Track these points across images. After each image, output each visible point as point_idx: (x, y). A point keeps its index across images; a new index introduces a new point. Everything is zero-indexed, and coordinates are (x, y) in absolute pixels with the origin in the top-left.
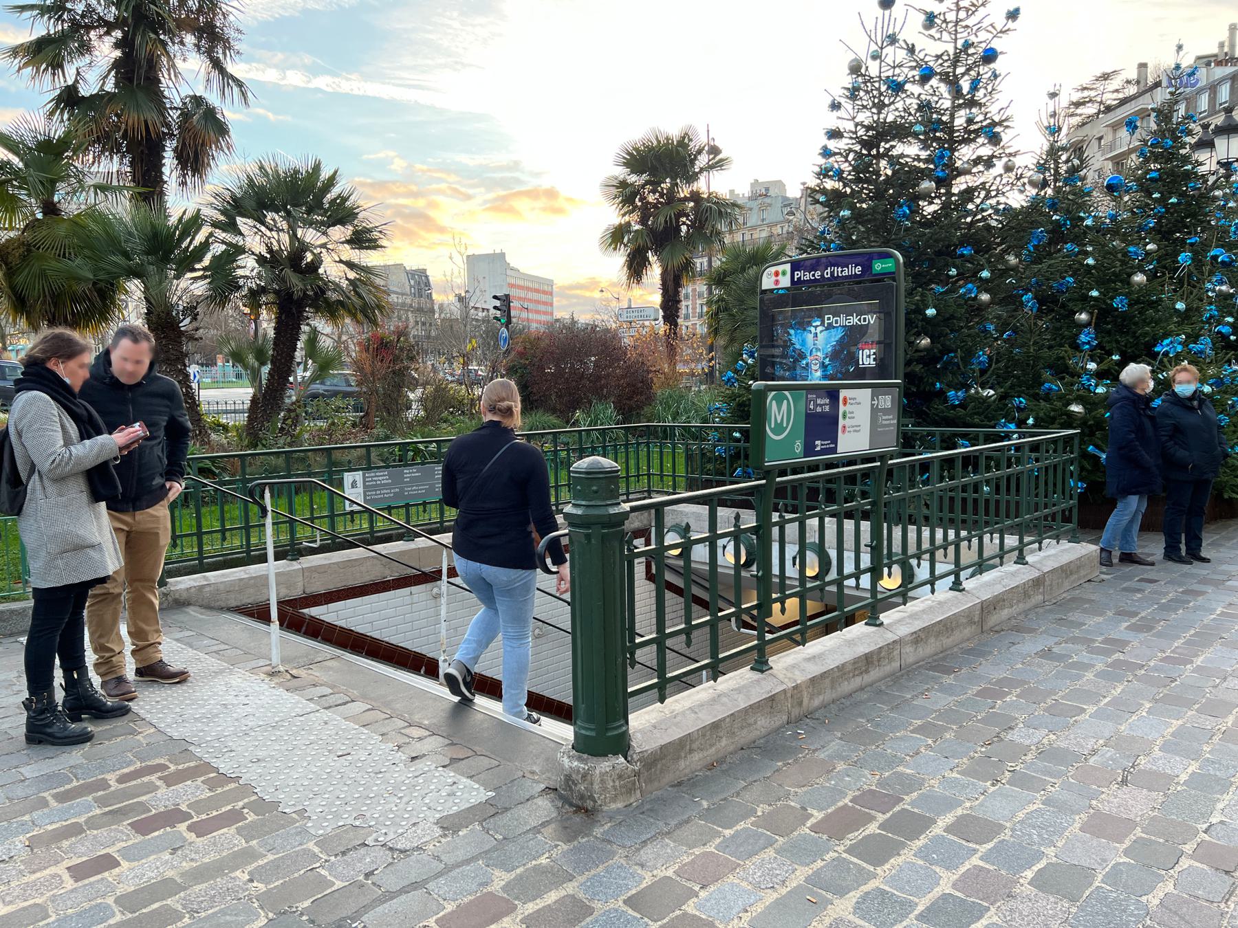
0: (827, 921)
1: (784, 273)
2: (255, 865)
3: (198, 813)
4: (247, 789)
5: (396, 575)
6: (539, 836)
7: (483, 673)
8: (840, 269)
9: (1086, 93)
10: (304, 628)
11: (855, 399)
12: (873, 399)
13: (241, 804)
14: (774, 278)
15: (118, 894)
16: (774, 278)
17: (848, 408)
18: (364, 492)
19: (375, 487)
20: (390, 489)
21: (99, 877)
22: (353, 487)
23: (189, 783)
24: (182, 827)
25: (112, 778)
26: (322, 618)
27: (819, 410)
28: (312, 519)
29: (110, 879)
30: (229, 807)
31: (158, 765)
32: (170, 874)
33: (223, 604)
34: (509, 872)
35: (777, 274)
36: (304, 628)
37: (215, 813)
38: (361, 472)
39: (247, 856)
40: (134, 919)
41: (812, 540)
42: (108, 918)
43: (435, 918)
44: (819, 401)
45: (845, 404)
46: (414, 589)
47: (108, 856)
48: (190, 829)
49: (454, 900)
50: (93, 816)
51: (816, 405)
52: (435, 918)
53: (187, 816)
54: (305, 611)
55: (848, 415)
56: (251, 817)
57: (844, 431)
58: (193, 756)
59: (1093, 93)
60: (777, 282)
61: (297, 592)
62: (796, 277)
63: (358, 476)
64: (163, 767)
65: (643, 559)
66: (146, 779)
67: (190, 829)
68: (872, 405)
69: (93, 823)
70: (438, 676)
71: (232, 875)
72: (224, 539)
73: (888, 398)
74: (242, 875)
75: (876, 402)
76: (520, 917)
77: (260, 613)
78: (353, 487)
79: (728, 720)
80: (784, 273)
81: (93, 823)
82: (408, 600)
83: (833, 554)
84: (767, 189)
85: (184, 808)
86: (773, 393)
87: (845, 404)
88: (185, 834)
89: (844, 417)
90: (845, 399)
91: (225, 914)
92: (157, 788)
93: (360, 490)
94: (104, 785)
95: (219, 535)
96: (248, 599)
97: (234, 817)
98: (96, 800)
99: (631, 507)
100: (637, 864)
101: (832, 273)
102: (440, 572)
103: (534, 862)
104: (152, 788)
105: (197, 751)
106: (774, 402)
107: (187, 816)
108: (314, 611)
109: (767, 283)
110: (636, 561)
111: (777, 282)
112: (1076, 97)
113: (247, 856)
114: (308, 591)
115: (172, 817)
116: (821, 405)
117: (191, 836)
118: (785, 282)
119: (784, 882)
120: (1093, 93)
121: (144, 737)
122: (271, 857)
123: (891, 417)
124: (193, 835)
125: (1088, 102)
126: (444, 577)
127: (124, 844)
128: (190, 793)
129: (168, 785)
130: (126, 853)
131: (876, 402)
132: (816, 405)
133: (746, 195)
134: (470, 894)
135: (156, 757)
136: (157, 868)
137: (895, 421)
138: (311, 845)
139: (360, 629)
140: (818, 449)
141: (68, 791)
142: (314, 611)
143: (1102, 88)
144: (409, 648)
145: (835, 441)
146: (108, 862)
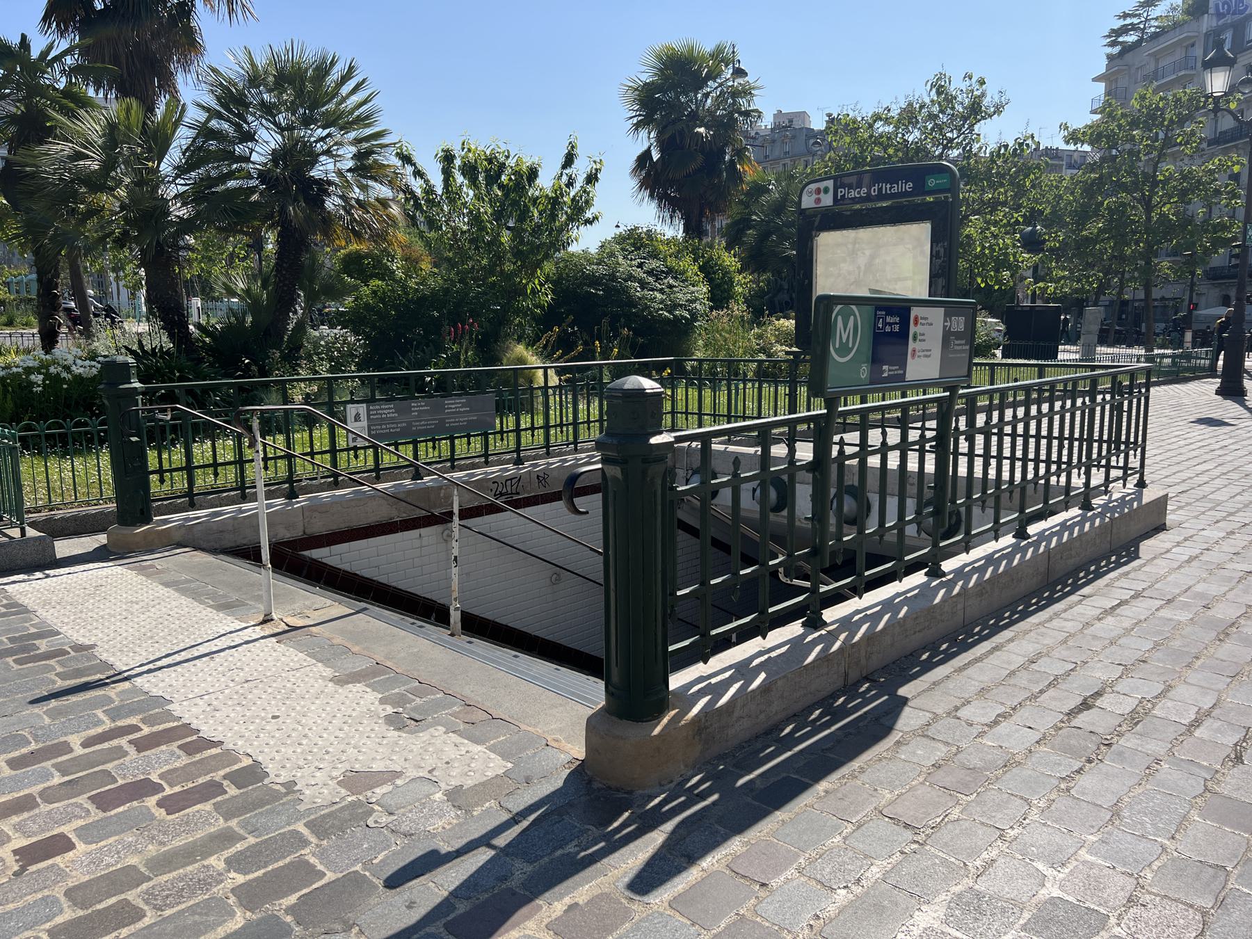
0: (916, 931)
1: (826, 190)
2: (233, 850)
3: (171, 786)
4: (229, 757)
5: (405, 516)
6: (566, 818)
7: (497, 620)
8: (888, 186)
9: (1128, 21)
10: (305, 572)
11: (926, 319)
12: (945, 321)
13: (222, 773)
14: (815, 196)
15: (71, 885)
16: (815, 196)
17: (919, 329)
18: (369, 427)
19: (382, 421)
20: (397, 423)
21: (50, 862)
22: (356, 420)
23: (164, 748)
24: (151, 801)
25: (75, 741)
26: (324, 561)
27: (888, 329)
28: (312, 454)
29: (62, 866)
30: (208, 778)
31: (129, 726)
32: (133, 860)
33: (217, 546)
34: (531, 863)
35: (818, 191)
36: (305, 572)
37: (190, 785)
38: (365, 405)
39: (227, 838)
40: (85, 917)
41: (850, 483)
42: (55, 915)
43: (444, 921)
44: (889, 319)
45: (916, 324)
46: (423, 531)
47: (62, 836)
48: (160, 804)
49: (469, 898)
50: (49, 788)
51: (885, 324)
52: (444, 921)
53: (157, 788)
54: (306, 553)
55: (919, 337)
56: (232, 791)
57: (913, 356)
58: (169, 716)
59: (1136, 21)
60: (818, 201)
61: (297, 533)
62: (839, 194)
63: (362, 408)
64: (135, 729)
65: (1006, 420)
66: (115, 743)
67: (160, 804)
68: (945, 327)
69: (49, 796)
70: (448, 623)
71: (206, 863)
72: (216, 474)
73: (962, 319)
74: (216, 862)
75: (948, 324)
76: (546, 921)
77: (250, 554)
78: (356, 420)
79: (780, 683)
80: (826, 190)
81: (49, 796)
82: (417, 543)
83: (875, 499)
84: (791, 121)
85: (155, 778)
86: (839, 307)
87: (916, 324)
88: (153, 811)
89: (915, 339)
90: (916, 319)
91: (194, 913)
92: (126, 754)
93: (364, 423)
94: (65, 748)
95: (210, 470)
96: (243, 540)
97: (214, 789)
98: (57, 767)
99: (675, 437)
100: (683, 855)
101: (880, 190)
102: (451, 514)
103: (559, 852)
104: (120, 753)
105: (176, 709)
106: (840, 318)
107: (157, 788)
108: (317, 554)
109: (807, 202)
110: (743, 486)
111: (818, 201)
112: (1118, 24)
113: (227, 838)
114: (309, 531)
115: (143, 788)
116: (890, 324)
117: (160, 813)
118: (827, 200)
119: (859, 880)
120: (1136, 21)
121: (116, 694)
122: (252, 840)
123: (963, 342)
124: (163, 811)
125: (1131, 30)
126: (456, 518)
127: (81, 823)
128: (168, 758)
129: (139, 751)
130: (83, 833)
131: (948, 324)
132: (885, 324)
133: (769, 127)
134: (485, 891)
135: (127, 716)
136: (118, 853)
137: (968, 347)
138: (300, 827)
139: (366, 573)
140: (885, 375)
141: (23, 756)
142: (317, 554)
143: (1145, 15)
144: (418, 593)
145: (903, 365)
146: (61, 845)
